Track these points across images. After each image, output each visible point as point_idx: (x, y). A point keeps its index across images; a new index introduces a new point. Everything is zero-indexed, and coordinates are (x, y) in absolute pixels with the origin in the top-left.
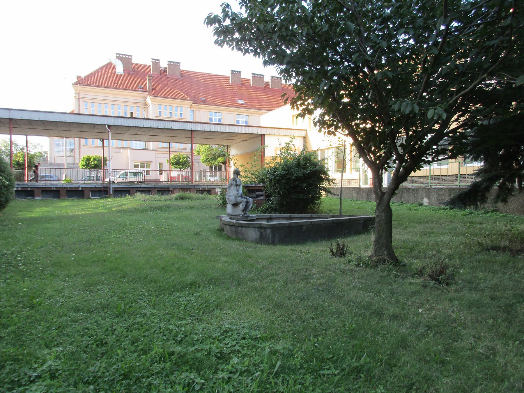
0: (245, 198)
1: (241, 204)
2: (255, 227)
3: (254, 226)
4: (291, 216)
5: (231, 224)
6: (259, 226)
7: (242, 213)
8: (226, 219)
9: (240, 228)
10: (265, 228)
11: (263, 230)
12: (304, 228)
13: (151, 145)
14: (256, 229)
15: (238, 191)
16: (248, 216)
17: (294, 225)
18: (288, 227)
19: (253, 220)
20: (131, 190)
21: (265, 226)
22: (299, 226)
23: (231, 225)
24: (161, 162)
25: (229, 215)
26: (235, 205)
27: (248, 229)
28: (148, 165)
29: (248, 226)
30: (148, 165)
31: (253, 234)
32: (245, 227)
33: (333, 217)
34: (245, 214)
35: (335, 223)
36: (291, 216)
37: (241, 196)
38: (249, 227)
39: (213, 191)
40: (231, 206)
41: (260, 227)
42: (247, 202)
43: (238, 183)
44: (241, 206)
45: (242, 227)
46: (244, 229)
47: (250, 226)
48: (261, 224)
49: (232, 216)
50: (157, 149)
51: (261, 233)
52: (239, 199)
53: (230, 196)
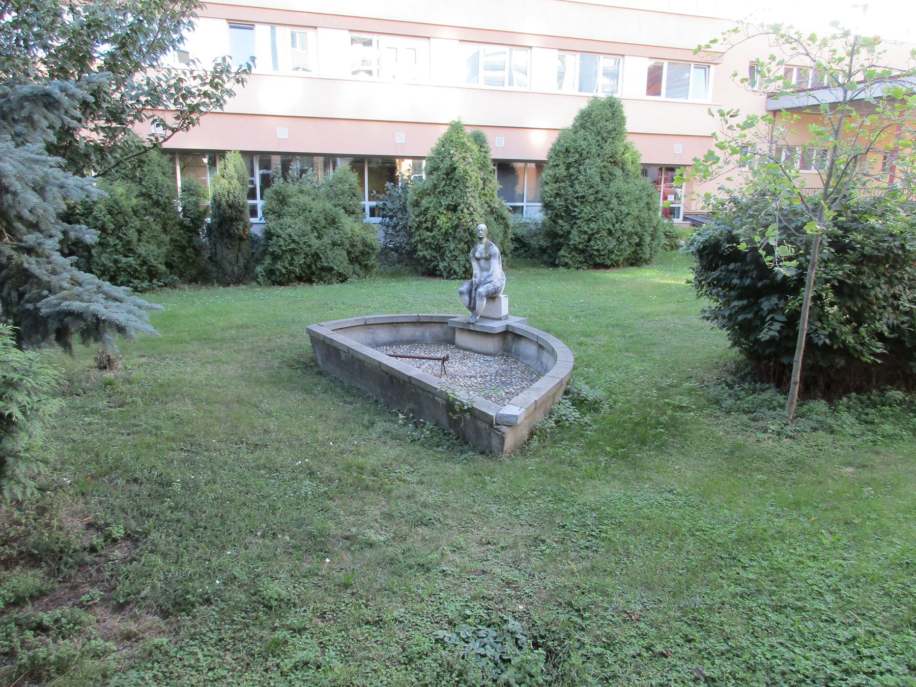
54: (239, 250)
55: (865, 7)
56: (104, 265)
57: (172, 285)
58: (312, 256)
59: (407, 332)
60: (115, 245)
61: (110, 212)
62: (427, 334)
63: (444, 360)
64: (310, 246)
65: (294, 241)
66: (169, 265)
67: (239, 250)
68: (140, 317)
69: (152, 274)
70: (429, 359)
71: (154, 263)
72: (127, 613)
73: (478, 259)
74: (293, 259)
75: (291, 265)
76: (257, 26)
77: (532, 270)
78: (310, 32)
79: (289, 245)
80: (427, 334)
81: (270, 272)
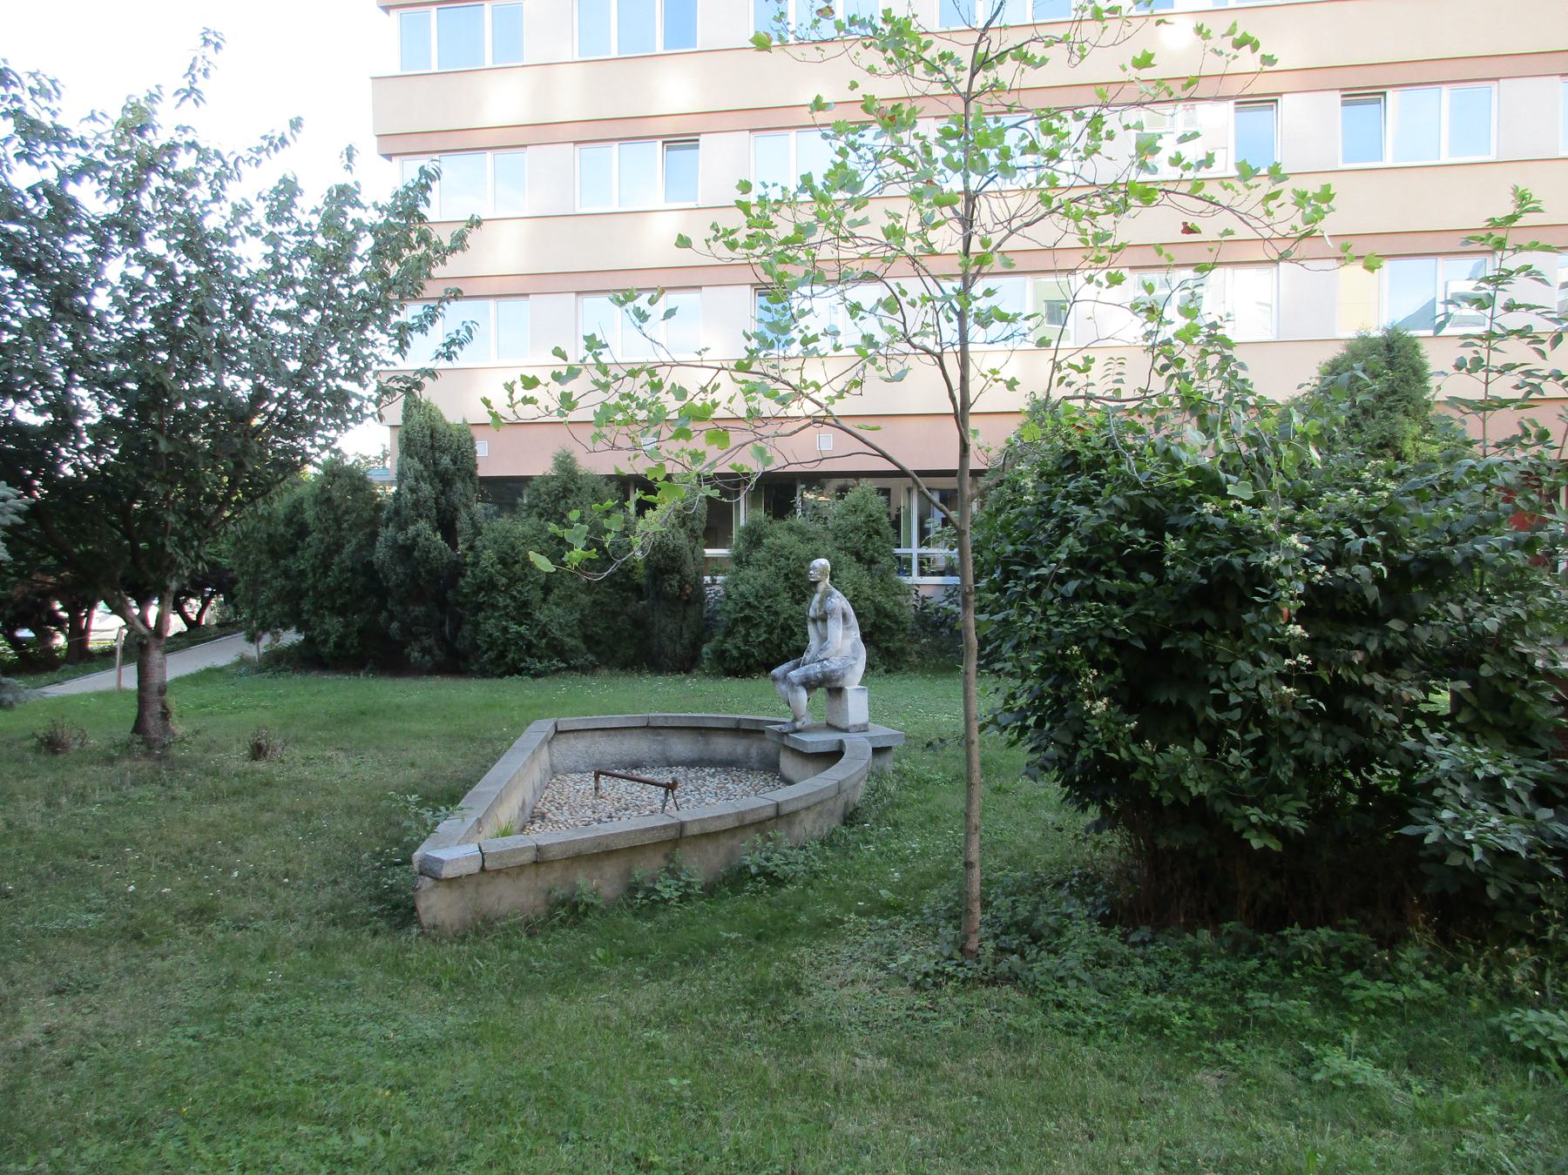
54: (684, 618)
55: (210, 40)
56: (490, 636)
57: (588, 670)
58: (783, 629)
59: (723, 746)
60: (506, 607)
61: (502, 561)
62: (754, 752)
63: (671, 787)
64: (776, 614)
65: (748, 604)
66: (588, 639)
67: (684, 618)
68: (211, 713)
69: (557, 649)
70: (645, 782)
71: (558, 634)
72: (67, 1001)
74: (748, 634)
75: (746, 642)
76: (702, 138)
77: (298, 677)
78: (1494, 84)
79: (742, 609)
80: (754, 752)
81: (721, 655)
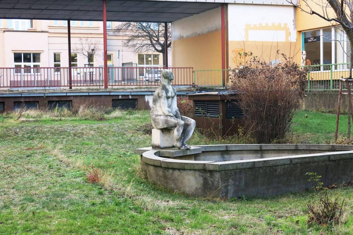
0: (182, 119)
1: (175, 130)
2: (195, 170)
3: (193, 168)
4: (261, 147)
5: (156, 164)
6: (201, 168)
7: (178, 144)
8: (150, 154)
9: (171, 171)
10: (211, 172)
11: (208, 175)
12: (279, 170)
13: (42, 24)
14: (197, 174)
15: (170, 106)
16: (188, 149)
17: (231, 168)
18: (301, 164)
19: (196, 156)
20: (6, 101)
21: (211, 168)
22: (271, 167)
23: (157, 166)
24: (57, 51)
25: (155, 147)
26: (166, 130)
27: (184, 173)
28: (36, 57)
29: (182, 168)
30: (36, 57)
31: (191, 182)
32: (179, 169)
33: (333, 149)
34: (183, 144)
35: (333, 161)
36: (261, 147)
37: (176, 116)
38: (184, 169)
39: (140, 102)
40: (159, 132)
41: (204, 170)
42: (186, 126)
43: (170, 94)
44: (176, 133)
45: (174, 169)
46: (177, 173)
47: (186, 167)
48: (204, 165)
49: (159, 150)
50: (50, 31)
51: (205, 179)
52: (173, 120)
53: (157, 115)
73: (168, 98)
